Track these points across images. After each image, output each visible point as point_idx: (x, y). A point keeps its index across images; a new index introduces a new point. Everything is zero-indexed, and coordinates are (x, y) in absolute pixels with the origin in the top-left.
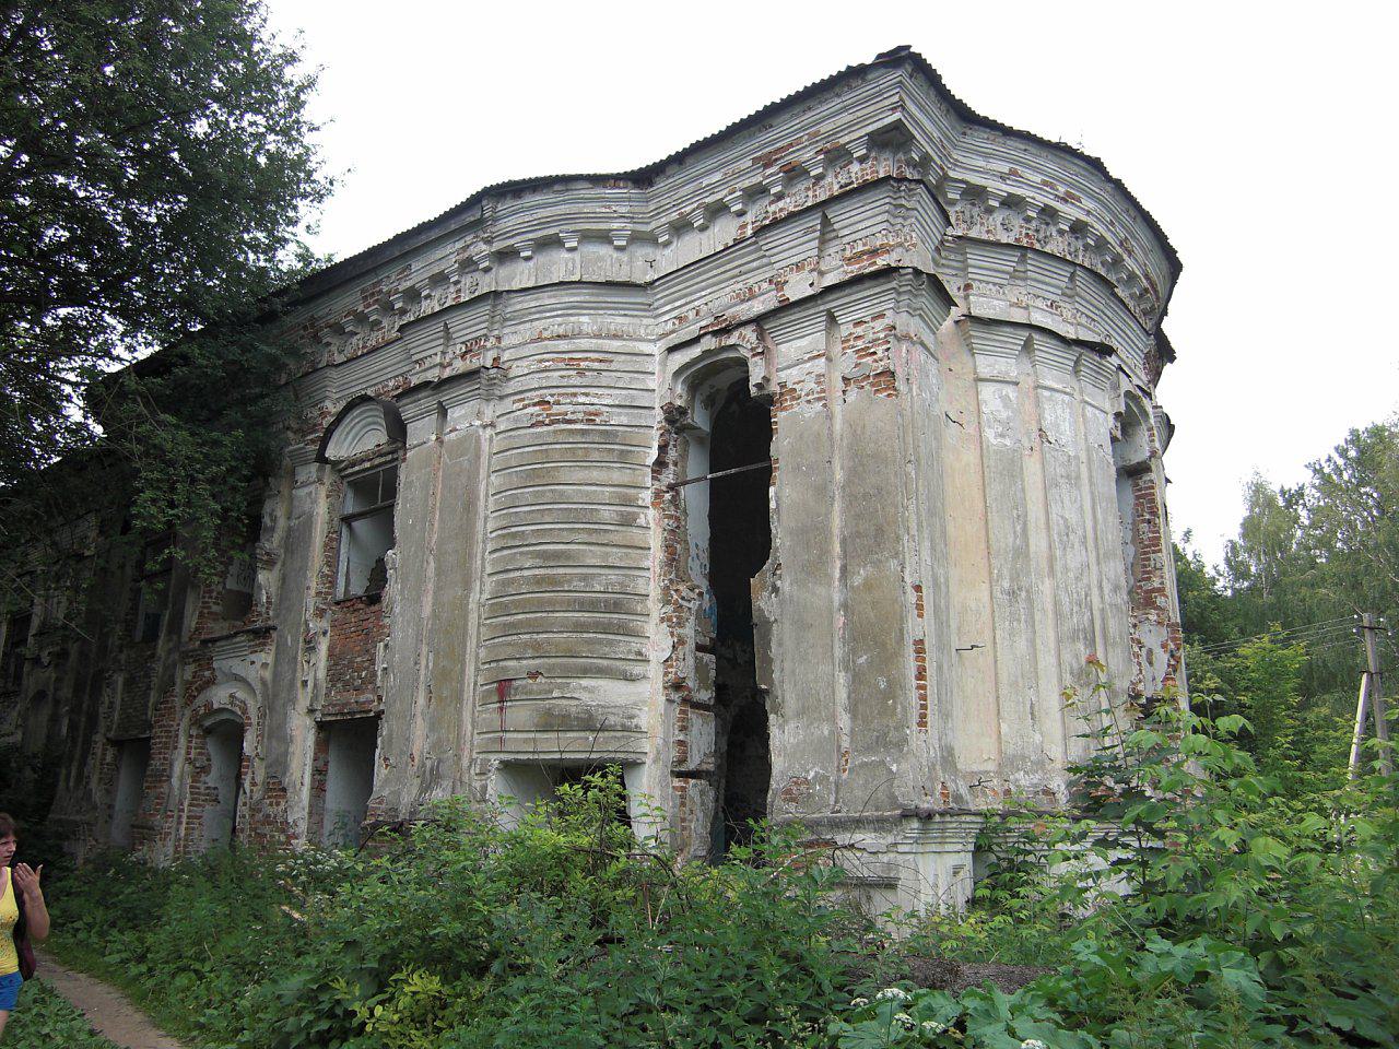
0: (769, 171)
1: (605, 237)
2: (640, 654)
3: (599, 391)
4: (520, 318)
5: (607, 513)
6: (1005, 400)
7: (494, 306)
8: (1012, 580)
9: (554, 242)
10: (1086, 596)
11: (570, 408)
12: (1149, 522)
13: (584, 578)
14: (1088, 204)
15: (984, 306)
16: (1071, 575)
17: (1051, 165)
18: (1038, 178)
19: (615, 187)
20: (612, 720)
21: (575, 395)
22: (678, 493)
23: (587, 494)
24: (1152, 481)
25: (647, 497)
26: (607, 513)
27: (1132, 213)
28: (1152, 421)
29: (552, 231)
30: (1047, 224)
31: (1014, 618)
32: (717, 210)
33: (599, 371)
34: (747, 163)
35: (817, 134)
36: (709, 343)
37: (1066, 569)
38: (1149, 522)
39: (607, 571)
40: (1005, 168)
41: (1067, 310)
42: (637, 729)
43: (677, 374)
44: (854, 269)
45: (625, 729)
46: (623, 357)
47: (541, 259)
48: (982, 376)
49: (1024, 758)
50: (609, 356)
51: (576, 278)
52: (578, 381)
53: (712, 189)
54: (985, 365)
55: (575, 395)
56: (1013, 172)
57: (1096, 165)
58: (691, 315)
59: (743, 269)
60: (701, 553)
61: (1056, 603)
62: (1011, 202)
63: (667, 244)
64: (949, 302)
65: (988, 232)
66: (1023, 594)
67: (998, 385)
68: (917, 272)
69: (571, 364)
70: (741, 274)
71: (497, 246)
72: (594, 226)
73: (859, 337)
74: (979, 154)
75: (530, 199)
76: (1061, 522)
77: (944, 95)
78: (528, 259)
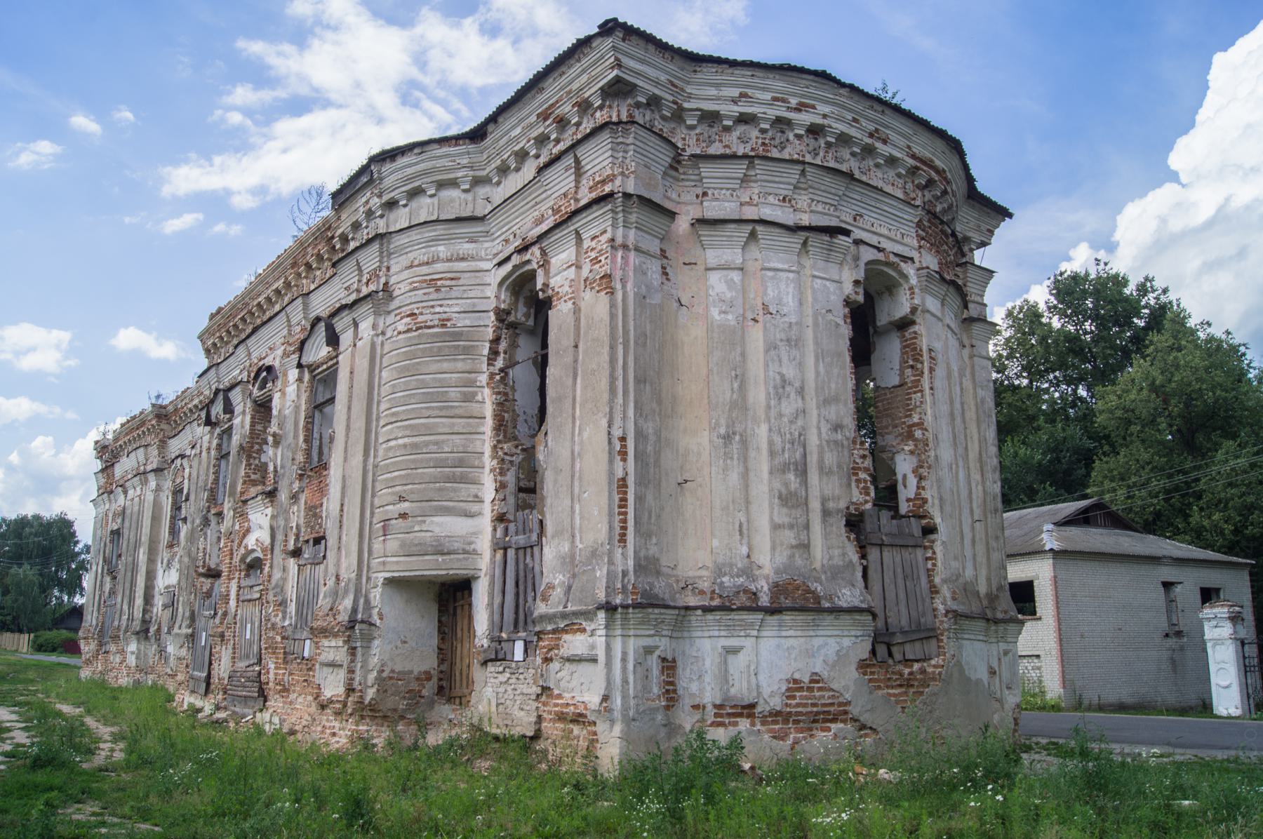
0: (548, 123)
1: (453, 183)
2: (476, 496)
3: (450, 302)
4: (401, 251)
5: (454, 393)
6: (730, 284)
7: (382, 245)
8: (728, 427)
9: (415, 193)
10: (800, 435)
11: (430, 317)
12: (912, 367)
13: (436, 443)
14: (823, 108)
15: (713, 210)
16: (785, 419)
17: (779, 84)
18: (768, 96)
19: (456, 145)
20: (456, 545)
21: (433, 307)
22: (507, 374)
23: (440, 380)
24: (915, 333)
25: (483, 379)
26: (454, 393)
27: (880, 108)
28: (914, 281)
29: (416, 184)
30: (783, 132)
31: (728, 456)
32: (522, 156)
33: (451, 287)
34: (533, 118)
35: (570, 92)
36: (516, 260)
37: (780, 415)
38: (912, 367)
39: (454, 437)
40: (735, 92)
41: (803, 200)
42: (475, 552)
43: (501, 284)
44: (594, 195)
45: (465, 552)
46: (468, 275)
47: (414, 204)
48: (710, 266)
49: (731, 565)
50: (458, 275)
51: (434, 218)
52: (434, 296)
53: (517, 139)
54: (712, 257)
55: (433, 307)
56: (742, 95)
57: (823, 76)
58: (511, 237)
59: (538, 200)
60: (529, 419)
61: (771, 443)
62: (744, 119)
63: (498, 183)
64: (671, 215)
65: (726, 146)
66: (737, 438)
67: (725, 272)
68: (627, 196)
69: (431, 283)
70: (537, 204)
71: (385, 198)
72: (445, 177)
73: (593, 249)
74: (711, 85)
75: (402, 161)
76: (778, 377)
77: (663, 47)
78: (405, 206)
